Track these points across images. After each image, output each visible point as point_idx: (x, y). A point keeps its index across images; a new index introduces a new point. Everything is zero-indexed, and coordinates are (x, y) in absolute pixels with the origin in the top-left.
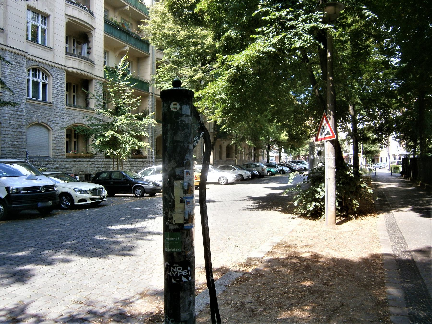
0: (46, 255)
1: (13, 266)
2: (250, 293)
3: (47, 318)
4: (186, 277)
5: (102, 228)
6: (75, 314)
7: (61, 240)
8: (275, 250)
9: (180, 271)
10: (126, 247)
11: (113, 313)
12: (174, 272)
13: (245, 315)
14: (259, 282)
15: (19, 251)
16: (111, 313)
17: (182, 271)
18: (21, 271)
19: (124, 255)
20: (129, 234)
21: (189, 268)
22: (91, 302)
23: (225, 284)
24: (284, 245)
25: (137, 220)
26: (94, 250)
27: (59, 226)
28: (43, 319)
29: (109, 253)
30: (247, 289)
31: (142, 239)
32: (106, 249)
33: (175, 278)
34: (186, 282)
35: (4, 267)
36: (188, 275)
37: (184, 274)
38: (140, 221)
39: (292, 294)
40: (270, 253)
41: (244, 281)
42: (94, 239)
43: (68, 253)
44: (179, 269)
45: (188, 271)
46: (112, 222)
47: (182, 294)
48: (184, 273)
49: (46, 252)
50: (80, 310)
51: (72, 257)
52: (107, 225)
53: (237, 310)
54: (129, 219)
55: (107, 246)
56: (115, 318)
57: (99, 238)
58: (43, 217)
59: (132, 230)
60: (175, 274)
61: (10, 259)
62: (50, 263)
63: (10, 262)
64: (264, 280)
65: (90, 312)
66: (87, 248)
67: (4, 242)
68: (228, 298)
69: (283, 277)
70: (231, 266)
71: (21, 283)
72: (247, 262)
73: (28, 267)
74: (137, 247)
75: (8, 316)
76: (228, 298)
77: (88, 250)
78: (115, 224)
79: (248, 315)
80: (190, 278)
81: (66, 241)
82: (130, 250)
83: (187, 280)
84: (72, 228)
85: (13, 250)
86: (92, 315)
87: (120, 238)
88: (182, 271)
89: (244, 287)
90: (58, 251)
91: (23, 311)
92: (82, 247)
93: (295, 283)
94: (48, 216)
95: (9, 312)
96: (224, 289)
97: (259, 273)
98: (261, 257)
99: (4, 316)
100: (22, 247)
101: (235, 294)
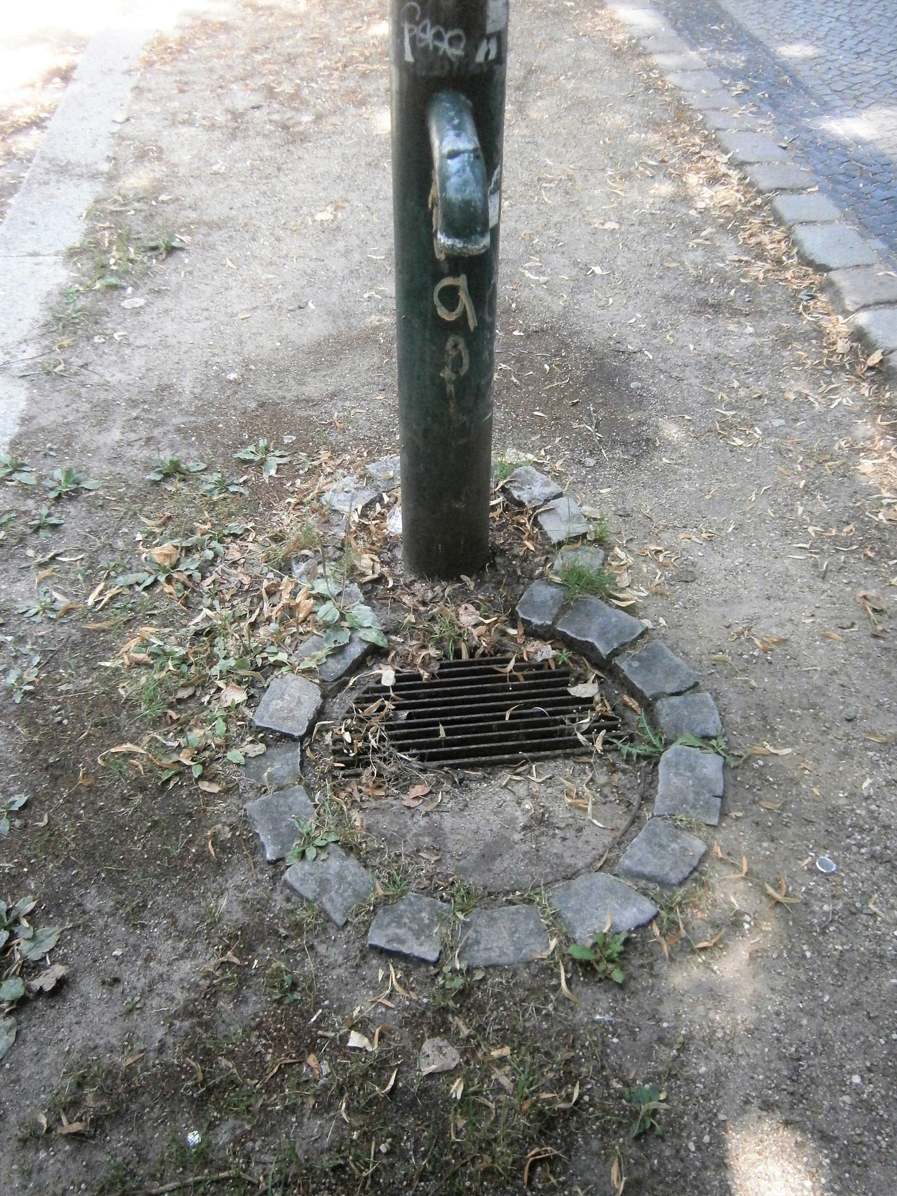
73: (430, 199)
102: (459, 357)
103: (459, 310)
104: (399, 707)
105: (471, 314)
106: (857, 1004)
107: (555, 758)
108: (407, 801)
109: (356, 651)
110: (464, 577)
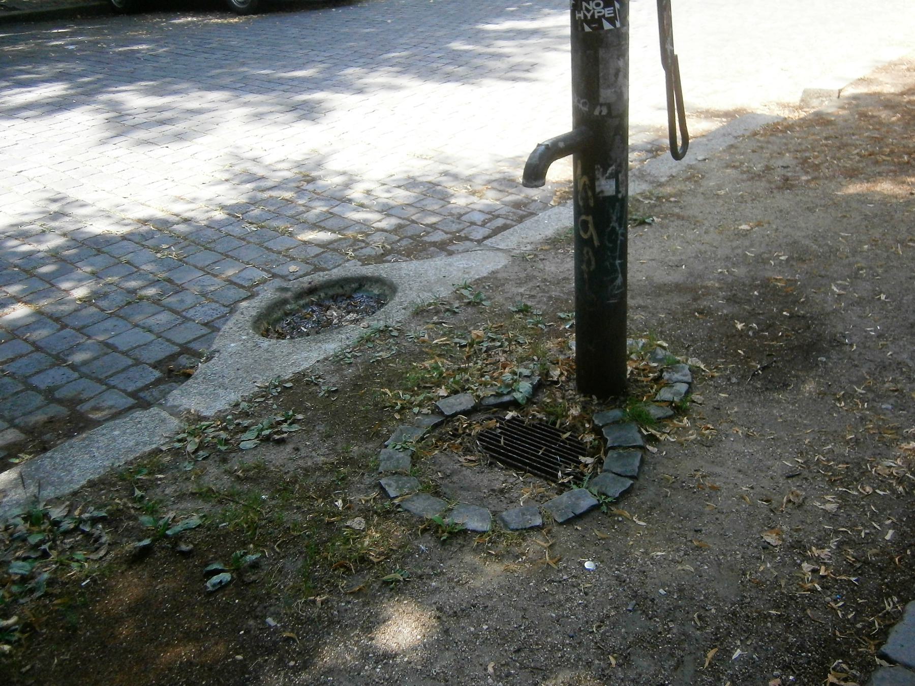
0: (350, 77)
1: (288, 95)
2: (790, 152)
3: (364, 178)
4: (612, 21)
5: (465, 27)
6: (417, 174)
7: (378, 49)
8: (877, 76)
9: (598, 9)
10: (519, 64)
11: (493, 178)
12: (588, 10)
13: (768, 186)
14: (818, 134)
15: (295, 70)
16: (488, 178)
17: (603, 8)
18: (305, 102)
19: (514, 79)
20: (526, 38)
21: (617, 5)
22: (447, 158)
23: (736, 135)
24: (904, 67)
25: (547, 11)
26: (450, 68)
27: (371, 24)
28: (357, 178)
29: (482, 76)
30: (786, 144)
31: (555, 50)
32: (476, 68)
33: (589, 23)
34: (610, 30)
35: (274, 94)
36: (615, 18)
37: (607, 16)
38: (555, 14)
39: (889, 155)
40: (862, 80)
41: (781, 131)
42: (447, 48)
43: (395, 75)
44: (598, 5)
45: (614, 10)
46: (486, 16)
47: (601, 52)
48: (606, 12)
49: (350, 71)
50: (427, 169)
51: (404, 80)
52: (477, 22)
53: (753, 178)
54: (529, 10)
55: (478, 62)
56: (495, 185)
57: (458, 45)
58: (335, 6)
59: (534, 32)
60: (589, 15)
61: (281, 82)
62: (360, 91)
63: (282, 88)
64: (830, 131)
65: (446, 174)
66: (435, 65)
67: (264, 52)
68: (737, 157)
69: (877, 127)
70: (762, 108)
71: (309, 122)
72: (802, 100)
73: (318, 95)
74: (544, 65)
75: (296, 170)
76: (737, 157)
77: (438, 69)
78: (496, 20)
79: (773, 186)
80: (618, 24)
81: (388, 52)
82: (528, 71)
83: (612, 27)
84: (398, 27)
85: (284, 66)
86: (451, 178)
87: (506, 47)
88: (603, 8)
89: (778, 141)
90: (373, 70)
91: (319, 165)
92: (422, 63)
93: (903, 138)
94: (343, 5)
95: (296, 164)
96: (732, 143)
97: (822, 118)
98: (836, 88)
99: (289, 170)
100: (300, 61)
101: (754, 151)
102: (589, 260)
103: (589, 234)
104: (500, 428)
105: (595, 237)
106: (525, 610)
107: (540, 477)
108: (462, 459)
109: (506, 398)
110: (594, 397)
